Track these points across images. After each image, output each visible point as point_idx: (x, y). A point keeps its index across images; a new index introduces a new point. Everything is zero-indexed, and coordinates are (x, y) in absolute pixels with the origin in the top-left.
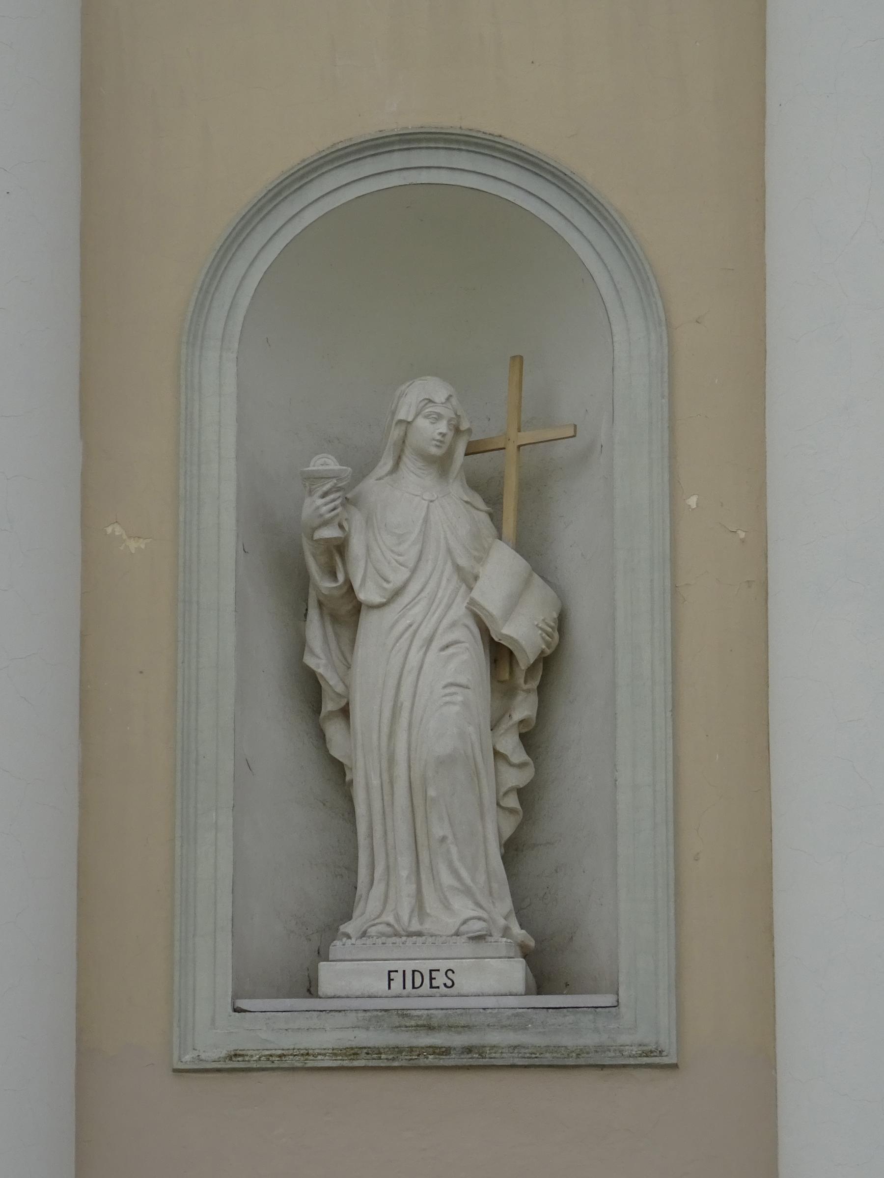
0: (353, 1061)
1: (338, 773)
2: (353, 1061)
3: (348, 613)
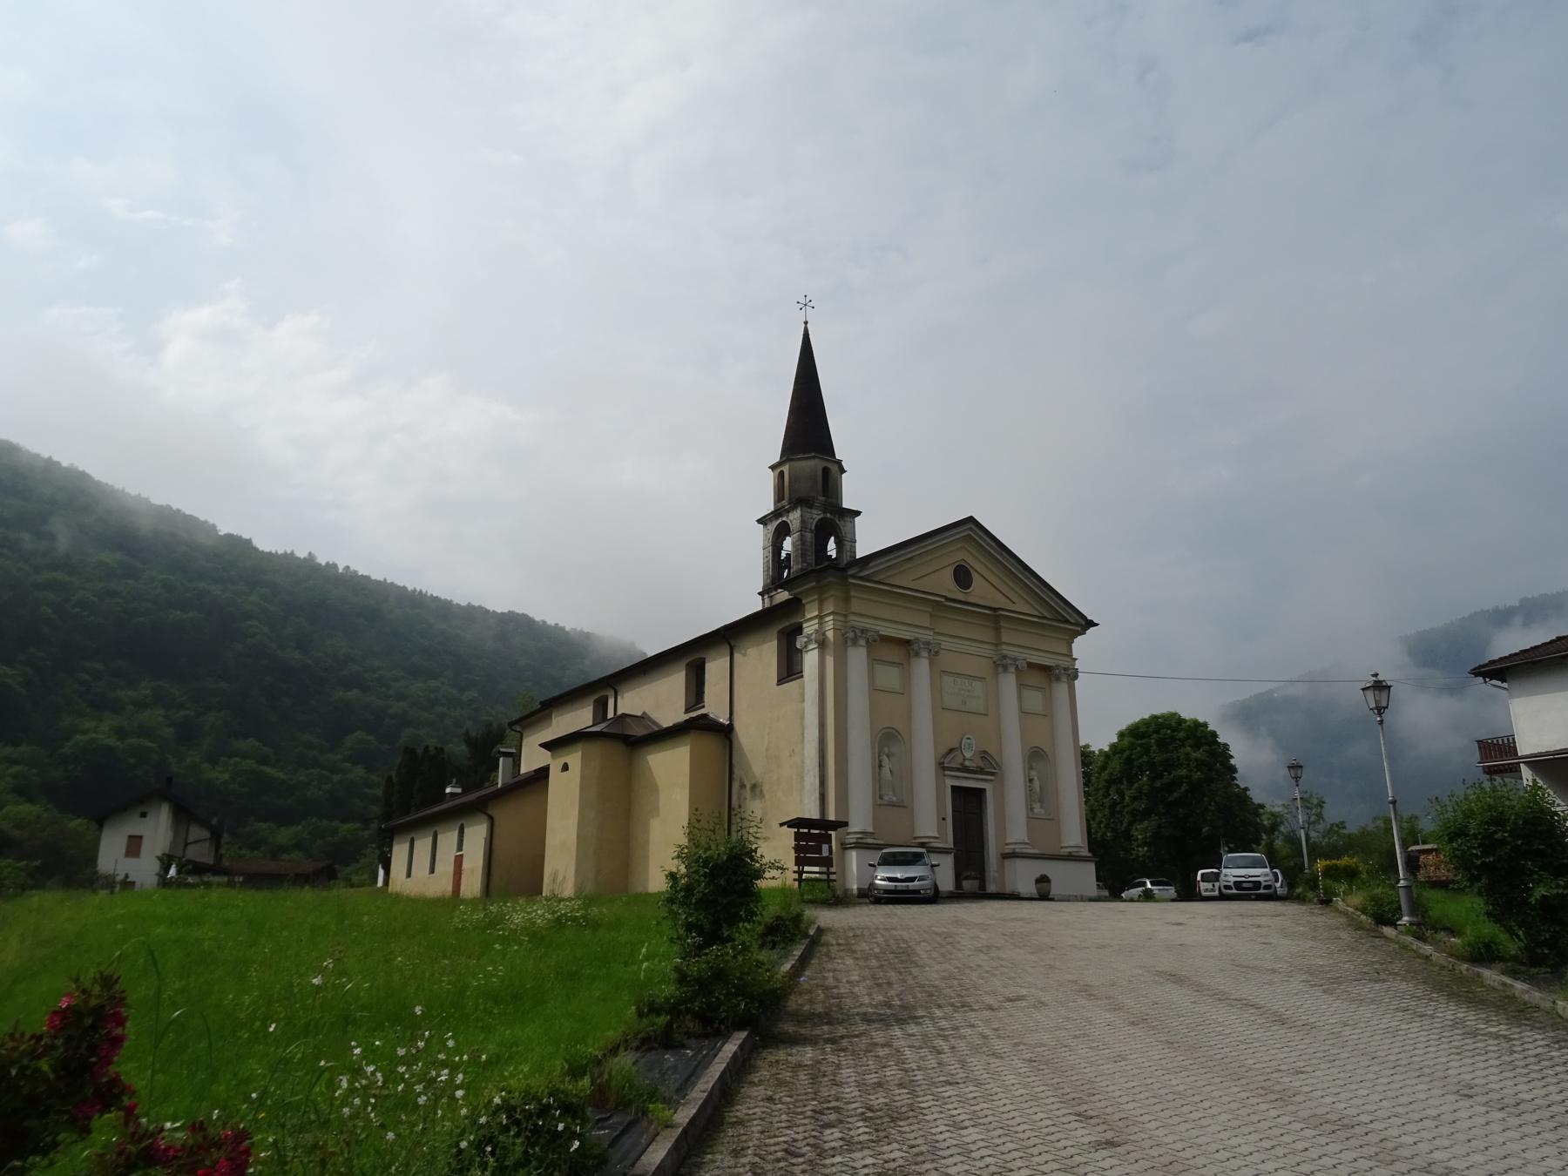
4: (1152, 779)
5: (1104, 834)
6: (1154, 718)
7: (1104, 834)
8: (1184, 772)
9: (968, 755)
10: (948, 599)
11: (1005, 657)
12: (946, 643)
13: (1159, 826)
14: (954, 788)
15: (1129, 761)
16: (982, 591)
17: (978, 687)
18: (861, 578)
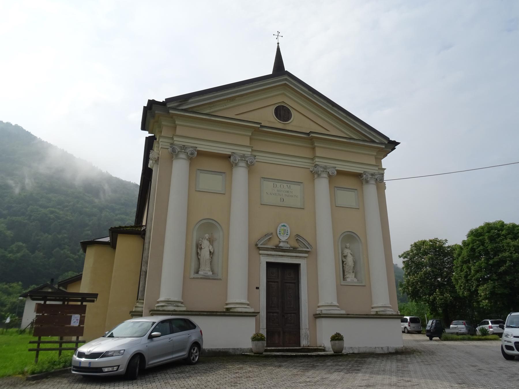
0: (201, 278)
1: (199, 259)
2: (201, 278)
3: (201, 248)
4: (487, 260)
5: (463, 293)
6: (488, 224)
7: (463, 293)
8: (507, 254)
9: (284, 238)
10: (262, 126)
11: (316, 166)
12: (260, 157)
13: (494, 287)
14: (269, 264)
15: (473, 250)
16: (298, 122)
17: (296, 189)
18: (185, 110)
